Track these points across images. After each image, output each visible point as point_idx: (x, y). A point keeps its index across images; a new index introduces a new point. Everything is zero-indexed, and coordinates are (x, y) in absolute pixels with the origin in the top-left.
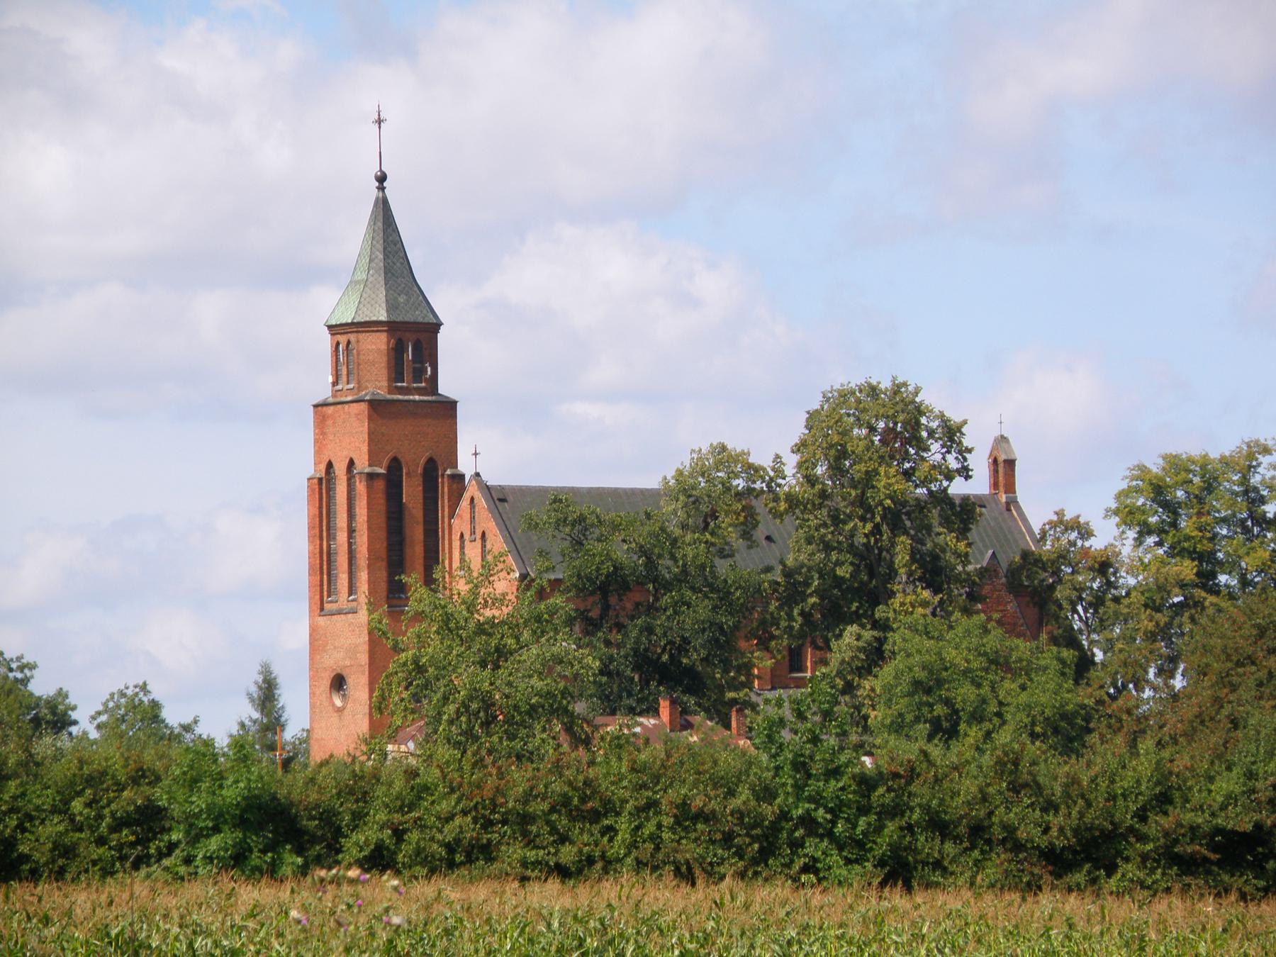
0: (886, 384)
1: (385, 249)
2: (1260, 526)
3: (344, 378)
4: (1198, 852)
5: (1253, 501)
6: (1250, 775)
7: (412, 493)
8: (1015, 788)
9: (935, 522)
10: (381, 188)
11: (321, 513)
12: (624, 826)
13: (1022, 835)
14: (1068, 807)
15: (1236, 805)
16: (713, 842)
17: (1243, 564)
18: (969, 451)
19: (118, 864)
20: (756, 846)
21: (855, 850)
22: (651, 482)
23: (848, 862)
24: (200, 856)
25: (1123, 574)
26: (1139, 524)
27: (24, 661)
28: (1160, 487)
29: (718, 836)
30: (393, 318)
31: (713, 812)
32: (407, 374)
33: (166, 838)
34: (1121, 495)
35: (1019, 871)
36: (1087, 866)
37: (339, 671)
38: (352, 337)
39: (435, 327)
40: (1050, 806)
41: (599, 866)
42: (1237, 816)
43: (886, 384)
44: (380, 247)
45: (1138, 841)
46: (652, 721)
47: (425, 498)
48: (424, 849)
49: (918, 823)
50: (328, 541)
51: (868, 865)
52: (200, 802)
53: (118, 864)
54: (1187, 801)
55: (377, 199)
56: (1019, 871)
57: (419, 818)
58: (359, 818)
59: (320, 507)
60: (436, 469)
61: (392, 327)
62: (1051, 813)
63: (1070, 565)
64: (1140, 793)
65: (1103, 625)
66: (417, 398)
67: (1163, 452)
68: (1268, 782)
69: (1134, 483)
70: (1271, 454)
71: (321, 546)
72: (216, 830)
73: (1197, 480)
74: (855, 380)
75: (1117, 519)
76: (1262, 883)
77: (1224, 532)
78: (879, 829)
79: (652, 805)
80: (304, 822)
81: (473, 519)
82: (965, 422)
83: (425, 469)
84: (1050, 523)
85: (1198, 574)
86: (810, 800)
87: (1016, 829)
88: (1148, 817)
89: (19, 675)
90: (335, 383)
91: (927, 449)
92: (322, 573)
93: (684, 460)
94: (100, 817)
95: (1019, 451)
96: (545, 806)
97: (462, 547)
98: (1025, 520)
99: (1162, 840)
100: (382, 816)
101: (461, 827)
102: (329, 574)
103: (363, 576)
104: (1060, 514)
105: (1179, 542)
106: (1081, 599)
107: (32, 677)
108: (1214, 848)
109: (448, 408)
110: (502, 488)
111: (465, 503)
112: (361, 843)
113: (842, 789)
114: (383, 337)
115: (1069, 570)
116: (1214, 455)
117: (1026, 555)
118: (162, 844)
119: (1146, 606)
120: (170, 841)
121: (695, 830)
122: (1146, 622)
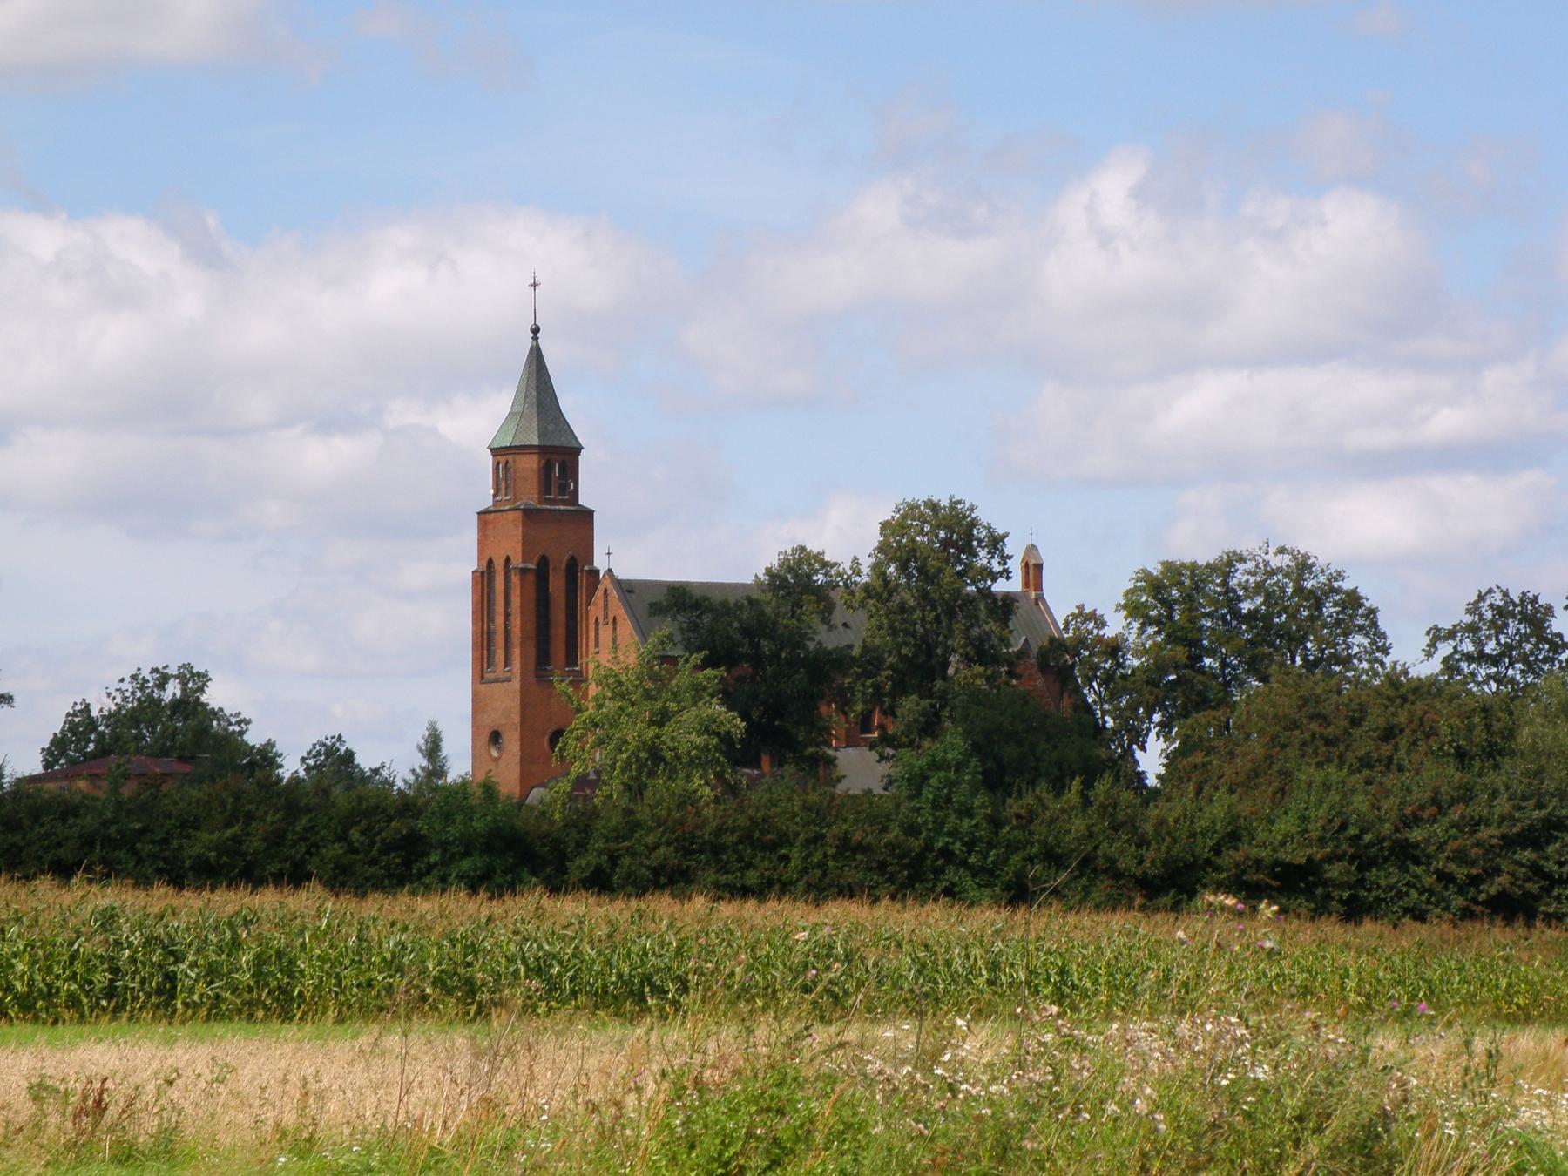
0: (945, 502)
1: (537, 387)
2: (1237, 620)
3: (503, 491)
4: (1263, 880)
5: (1232, 600)
6: (1304, 819)
7: (557, 584)
8: (1115, 828)
9: (983, 615)
10: (535, 338)
11: (482, 601)
12: (796, 855)
13: (1121, 865)
14: (1158, 843)
15: (1292, 843)
16: (871, 869)
17: (1224, 650)
18: (1010, 558)
19: (387, 881)
20: (906, 873)
21: (986, 875)
22: (749, 580)
23: (980, 886)
24: (454, 875)
25: (1129, 656)
26: (1142, 617)
27: (242, 717)
28: (1159, 587)
29: (874, 865)
30: (543, 443)
31: (870, 845)
32: (554, 488)
33: (426, 860)
34: (1129, 593)
35: (1119, 895)
36: (1172, 892)
37: (496, 728)
38: (510, 458)
39: (577, 450)
40: (1143, 843)
41: (777, 887)
42: (1293, 851)
43: (945, 502)
44: (533, 385)
45: (1213, 871)
46: (756, 772)
47: (567, 590)
48: (635, 872)
49: (1036, 856)
50: (488, 622)
51: (997, 889)
52: (453, 831)
53: (387, 881)
54: (1253, 839)
55: (532, 347)
56: (1119, 895)
57: (48, 835)
58: (581, 846)
59: (482, 596)
60: (577, 566)
61: (542, 450)
62: (1145, 847)
63: (1087, 649)
64: (1216, 832)
65: (1114, 696)
66: (562, 507)
67: (1161, 560)
68: (1319, 825)
69: (1139, 584)
70: (1245, 562)
71: (482, 626)
72: (467, 854)
73: (1187, 582)
74: (920, 496)
75: (1125, 612)
76: (1312, 906)
77: (1209, 624)
78: (1006, 861)
79: (818, 839)
80: (537, 848)
81: (606, 606)
82: (1006, 535)
83: (568, 565)
84: (1073, 614)
85: (1189, 657)
86: (950, 834)
87: (1116, 861)
88: (1221, 852)
89: (237, 729)
90: (495, 495)
91: (975, 555)
92: (483, 649)
93: (774, 561)
94: (373, 843)
95: (1046, 557)
96: (735, 838)
97: (597, 629)
98: (1050, 613)
99: (1234, 870)
100: (601, 844)
101: (665, 855)
102: (488, 650)
103: (516, 652)
104: (1081, 608)
105: (1174, 632)
106: (1096, 677)
107: (247, 729)
108: (1275, 877)
109: (588, 515)
110: (629, 582)
111: (599, 594)
112: (583, 866)
113: (976, 826)
114: (535, 458)
115: (1087, 653)
116: (1202, 562)
117: (1052, 640)
118: (422, 866)
119: (1147, 683)
120: (429, 863)
121: (855, 860)
122: (1147, 696)
